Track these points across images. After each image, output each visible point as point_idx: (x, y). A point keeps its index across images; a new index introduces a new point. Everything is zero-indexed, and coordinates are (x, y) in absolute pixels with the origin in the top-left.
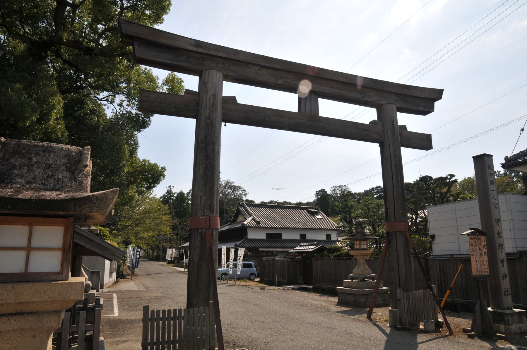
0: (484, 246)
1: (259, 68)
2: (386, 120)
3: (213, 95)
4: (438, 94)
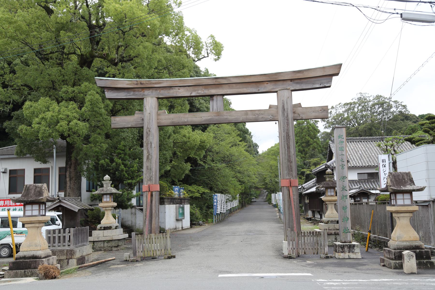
4: (336, 70)
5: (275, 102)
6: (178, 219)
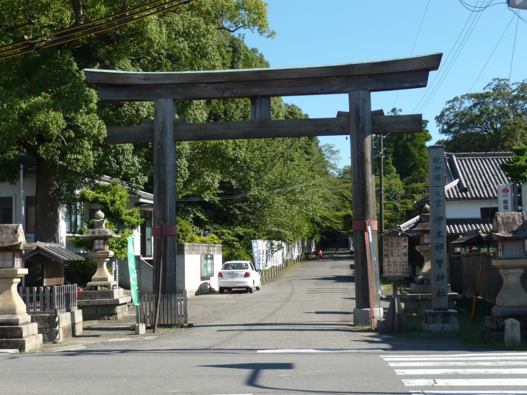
0: (405, 246)
1: (205, 84)
2: (359, 105)
3: (162, 122)
4: (434, 61)
5: (345, 108)
6: (203, 276)
